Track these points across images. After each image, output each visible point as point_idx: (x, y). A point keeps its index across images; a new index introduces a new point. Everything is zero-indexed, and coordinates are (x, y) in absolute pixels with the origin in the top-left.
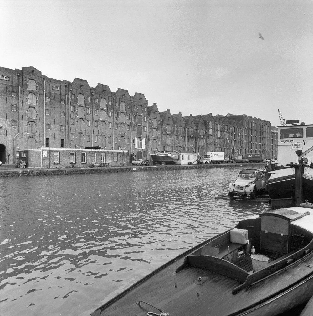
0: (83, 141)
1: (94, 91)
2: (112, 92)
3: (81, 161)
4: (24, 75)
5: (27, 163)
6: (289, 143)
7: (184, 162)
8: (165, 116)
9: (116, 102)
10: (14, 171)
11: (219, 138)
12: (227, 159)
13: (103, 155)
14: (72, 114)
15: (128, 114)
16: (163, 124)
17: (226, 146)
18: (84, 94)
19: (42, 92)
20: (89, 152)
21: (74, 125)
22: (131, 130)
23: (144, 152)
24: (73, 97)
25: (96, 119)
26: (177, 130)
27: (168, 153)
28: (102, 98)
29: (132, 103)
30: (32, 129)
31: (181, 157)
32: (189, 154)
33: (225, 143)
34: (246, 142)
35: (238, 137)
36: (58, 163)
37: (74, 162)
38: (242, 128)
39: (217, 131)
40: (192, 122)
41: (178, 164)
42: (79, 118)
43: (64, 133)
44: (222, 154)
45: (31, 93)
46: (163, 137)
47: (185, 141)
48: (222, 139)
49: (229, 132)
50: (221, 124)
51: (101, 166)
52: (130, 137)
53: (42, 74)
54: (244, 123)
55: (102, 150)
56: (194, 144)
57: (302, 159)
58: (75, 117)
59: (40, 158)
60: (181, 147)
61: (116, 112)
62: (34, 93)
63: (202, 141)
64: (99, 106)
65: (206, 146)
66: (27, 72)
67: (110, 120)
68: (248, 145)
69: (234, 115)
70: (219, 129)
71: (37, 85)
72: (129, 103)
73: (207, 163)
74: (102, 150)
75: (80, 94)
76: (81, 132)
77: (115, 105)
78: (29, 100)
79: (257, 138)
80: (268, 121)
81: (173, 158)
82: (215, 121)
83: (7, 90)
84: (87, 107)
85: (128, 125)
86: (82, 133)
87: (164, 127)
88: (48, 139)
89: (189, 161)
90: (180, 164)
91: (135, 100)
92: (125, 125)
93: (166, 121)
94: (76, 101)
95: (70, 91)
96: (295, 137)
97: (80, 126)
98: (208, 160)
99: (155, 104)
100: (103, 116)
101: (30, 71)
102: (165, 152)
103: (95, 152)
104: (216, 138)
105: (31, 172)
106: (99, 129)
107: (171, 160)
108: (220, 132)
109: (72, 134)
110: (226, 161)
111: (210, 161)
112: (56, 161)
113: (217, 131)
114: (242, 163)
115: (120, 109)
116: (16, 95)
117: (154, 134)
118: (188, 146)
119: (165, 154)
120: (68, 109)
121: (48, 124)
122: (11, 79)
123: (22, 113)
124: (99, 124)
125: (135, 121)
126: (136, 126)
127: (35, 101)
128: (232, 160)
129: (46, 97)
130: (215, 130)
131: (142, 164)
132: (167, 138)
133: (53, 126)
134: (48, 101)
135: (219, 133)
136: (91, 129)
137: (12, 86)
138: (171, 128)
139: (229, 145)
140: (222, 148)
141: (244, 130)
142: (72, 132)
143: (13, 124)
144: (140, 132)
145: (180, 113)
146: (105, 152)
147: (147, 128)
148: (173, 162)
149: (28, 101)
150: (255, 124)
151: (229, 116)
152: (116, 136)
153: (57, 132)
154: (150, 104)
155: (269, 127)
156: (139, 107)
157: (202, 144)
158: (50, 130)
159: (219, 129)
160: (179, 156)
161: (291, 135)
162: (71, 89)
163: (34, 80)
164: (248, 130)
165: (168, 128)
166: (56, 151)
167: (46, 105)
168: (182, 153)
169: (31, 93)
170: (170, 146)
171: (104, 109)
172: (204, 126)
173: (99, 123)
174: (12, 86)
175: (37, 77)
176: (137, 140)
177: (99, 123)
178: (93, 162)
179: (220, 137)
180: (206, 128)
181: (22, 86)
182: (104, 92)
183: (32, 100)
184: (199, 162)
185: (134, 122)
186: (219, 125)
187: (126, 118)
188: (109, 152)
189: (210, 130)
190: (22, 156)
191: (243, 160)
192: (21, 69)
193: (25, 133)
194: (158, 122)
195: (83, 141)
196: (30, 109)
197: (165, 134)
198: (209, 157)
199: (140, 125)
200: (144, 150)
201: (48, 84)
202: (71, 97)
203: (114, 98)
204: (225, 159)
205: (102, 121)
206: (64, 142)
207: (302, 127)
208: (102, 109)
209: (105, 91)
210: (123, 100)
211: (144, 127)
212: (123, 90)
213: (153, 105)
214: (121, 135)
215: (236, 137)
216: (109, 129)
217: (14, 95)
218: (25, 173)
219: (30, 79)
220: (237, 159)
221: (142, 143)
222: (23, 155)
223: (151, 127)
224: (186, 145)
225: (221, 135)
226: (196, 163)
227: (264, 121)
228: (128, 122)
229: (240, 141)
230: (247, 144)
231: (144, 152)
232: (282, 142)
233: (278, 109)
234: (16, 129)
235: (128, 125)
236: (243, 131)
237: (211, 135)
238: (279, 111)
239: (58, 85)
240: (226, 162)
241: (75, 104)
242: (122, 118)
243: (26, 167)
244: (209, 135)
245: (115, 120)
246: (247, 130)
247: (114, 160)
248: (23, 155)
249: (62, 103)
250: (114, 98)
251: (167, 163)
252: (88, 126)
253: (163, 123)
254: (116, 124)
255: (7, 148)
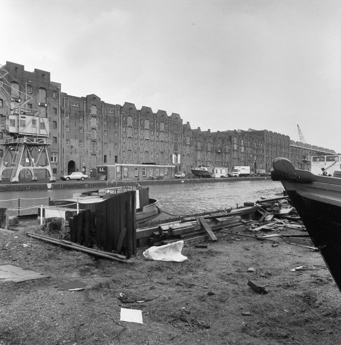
0: (131, 157)
1: (140, 113)
2: (154, 114)
3: (142, 174)
4: (88, 101)
5: (106, 177)
6: (317, 164)
7: (218, 176)
8: (197, 134)
9: (157, 122)
10: (103, 183)
11: (243, 153)
12: (253, 173)
13: (157, 170)
14: (123, 134)
15: (166, 133)
16: (195, 141)
17: (249, 161)
18: (132, 116)
19: (101, 115)
20: (148, 167)
21: (125, 143)
22: (168, 146)
23: (180, 166)
24: (124, 119)
25: (142, 138)
26: (207, 146)
27: (205, 168)
28: (146, 119)
29: (169, 122)
30: (94, 147)
31: (215, 171)
32: (221, 168)
33: (248, 158)
34: (267, 156)
35: (260, 151)
36: (127, 176)
37: (137, 176)
38: (263, 143)
39: (241, 146)
40: (220, 138)
41: (213, 178)
42: (129, 137)
43: (117, 151)
44: (249, 168)
45: (93, 117)
46: (195, 153)
47: (214, 156)
48: (245, 153)
49: (251, 147)
50: (245, 139)
51: (158, 179)
52: (168, 153)
53: (101, 100)
54: (265, 137)
55: (157, 166)
56: (221, 159)
57: (324, 172)
58: (125, 136)
59: (115, 172)
60: (210, 161)
61: (157, 132)
62: (95, 117)
63: (227, 156)
64: (144, 126)
65: (231, 161)
66: (90, 99)
67: (152, 139)
68: (269, 159)
69: (255, 130)
70: (242, 144)
71: (97, 110)
72: (167, 122)
73: (236, 176)
74: (157, 166)
75: (129, 116)
76: (130, 149)
77: (156, 125)
78: (91, 123)
79: (277, 153)
80: (287, 136)
81: (209, 172)
82: (239, 137)
83: (76, 115)
84: (135, 127)
85: (166, 142)
86: (131, 150)
87: (196, 143)
88: (105, 156)
89: (222, 175)
90: (215, 178)
91: (172, 120)
92: (164, 142)
93: (198, 138)
94: (126, 122)
95: (122, 113)
96: (320, 161)
97: (129, 144)
98: (237, 174)
99: (188, 123)
100: (147, 135)
101: (92, 98)
102: (202, 167)
103: (152, 167)
104: (240, 153)
105: (114, 183)
106: (144, 147)
107: (208, 174)
108: (243, 147)
109: (123, 151)
110: (252, 175)
111: (238, 174)
112: (126, 175)
113: (241, 146)
114: (265, 176)
115: (161, 128)
116: (82, 119)
117: (188, 150)
118: (216, 161)
119: (203, 168)
120: (120, 130)
121: (105, 143)
122: (79, 106)
123: (87, 134)
124: (144, 142)
125: (172, 139)
126: (173, 143)
127: (96, 124)
128: (257, 173)
129: (104, 120)
130: (239, 145)
131: (185, 177)
132: (198, 154)
133: (109, 145)
134: (106, 123)
135: (243, 148)
136: (154, 148)
137: (80, 112)
138: (202, 144)
139: (252, 159)
140: (245, 162)
141: (265, 145)
142: (123, 150)
143: (80, 144)
144: (176, 149)
145: (199, 128)
146: (159, 168)
147: (181, 144)
148: (209, 175)
149: (91, 124)
150: (275, 139)
151: (251, 131)
152: (157, 152)
153: (112, 150)
154: (184, 123)
155: (288, 141)
156: (175, 126)
157: (228, 159)
158: (107, 148)
159: (242, 144)
160: (213, 171)
161: (318, 160)
162: (123, 112)
163: (95, 106)
164: (269, 145)
165: (199, 144)
166: (126, 167)
167: (104, 126)
168: (216, 167)
169: (93, 117)
170: (201, 161)
171: (147, 128)
172: (230, 142)
173: (144, 141)
174: (80, 112)
175: (97, 103)
176: (174, 156)
177: (144, 141)
178: (151, 176)
179: (243, 151)
180: (231, 144)
181: (87, 111)
182: (147, 114)
183: (94, 123)
184: (230, 176)
185: (171, 140)
186: (242, 141)
187: (165, 136)
188: (161, 167)
189: (235, 146)
190: (100, 171)
191: (266, 173)
192: (86, 97)
193: (90, 151)
194: (191, 139)
195: (131, 157)
196: (92, 130)
197: (197, 150)
198: (237, 171)
199: (176, 142)
200: (179, 165)
201: (106, 109)
202: (122, 119)
203: (155, 119)
204: (250, 172)
205: (146, 139)
206: (118, 158)
207: (324, 156)
208: (146, 129)
209: (148, 112)
210: (163, 120)
211: (179, 144)
212: (162, 111)
213: (186, 123)
214: (161, 152)
215: (258, 151)
216: (152, 146)
217: (81, 120)
218: (110, 184)
219: (93, 105)
220: (261, 172)
221: (177, 158)
222: (101, 170)
223: (185, 144)
224: (214, 160)
225: (245, 150)
226: (227, 176)
227: (284, 136)
228: (167, 140)
229: (262, 155)
230: (268, 158)
231: (180, 166)
232: (313, 163)
233: (298, 125)
234: (83, 148)
235: (166, 142)
236: (264, 145)
237: (235, 150)
238: (298, 126)
239: (113, 109)
240: (252, 176)
241: (125, 125)
242: (162, 136)
243: (106, 179)
244: (234, 150)
245: (157, 138)
246: (268, 145)
247: (166, 174)
248: (101, 170)
249: (116, 125)
250: (155, 119)
251: (203, 176)
252: (136, 144)
253: (195, 140)
254: (157, 141)
255: (76, 164)
